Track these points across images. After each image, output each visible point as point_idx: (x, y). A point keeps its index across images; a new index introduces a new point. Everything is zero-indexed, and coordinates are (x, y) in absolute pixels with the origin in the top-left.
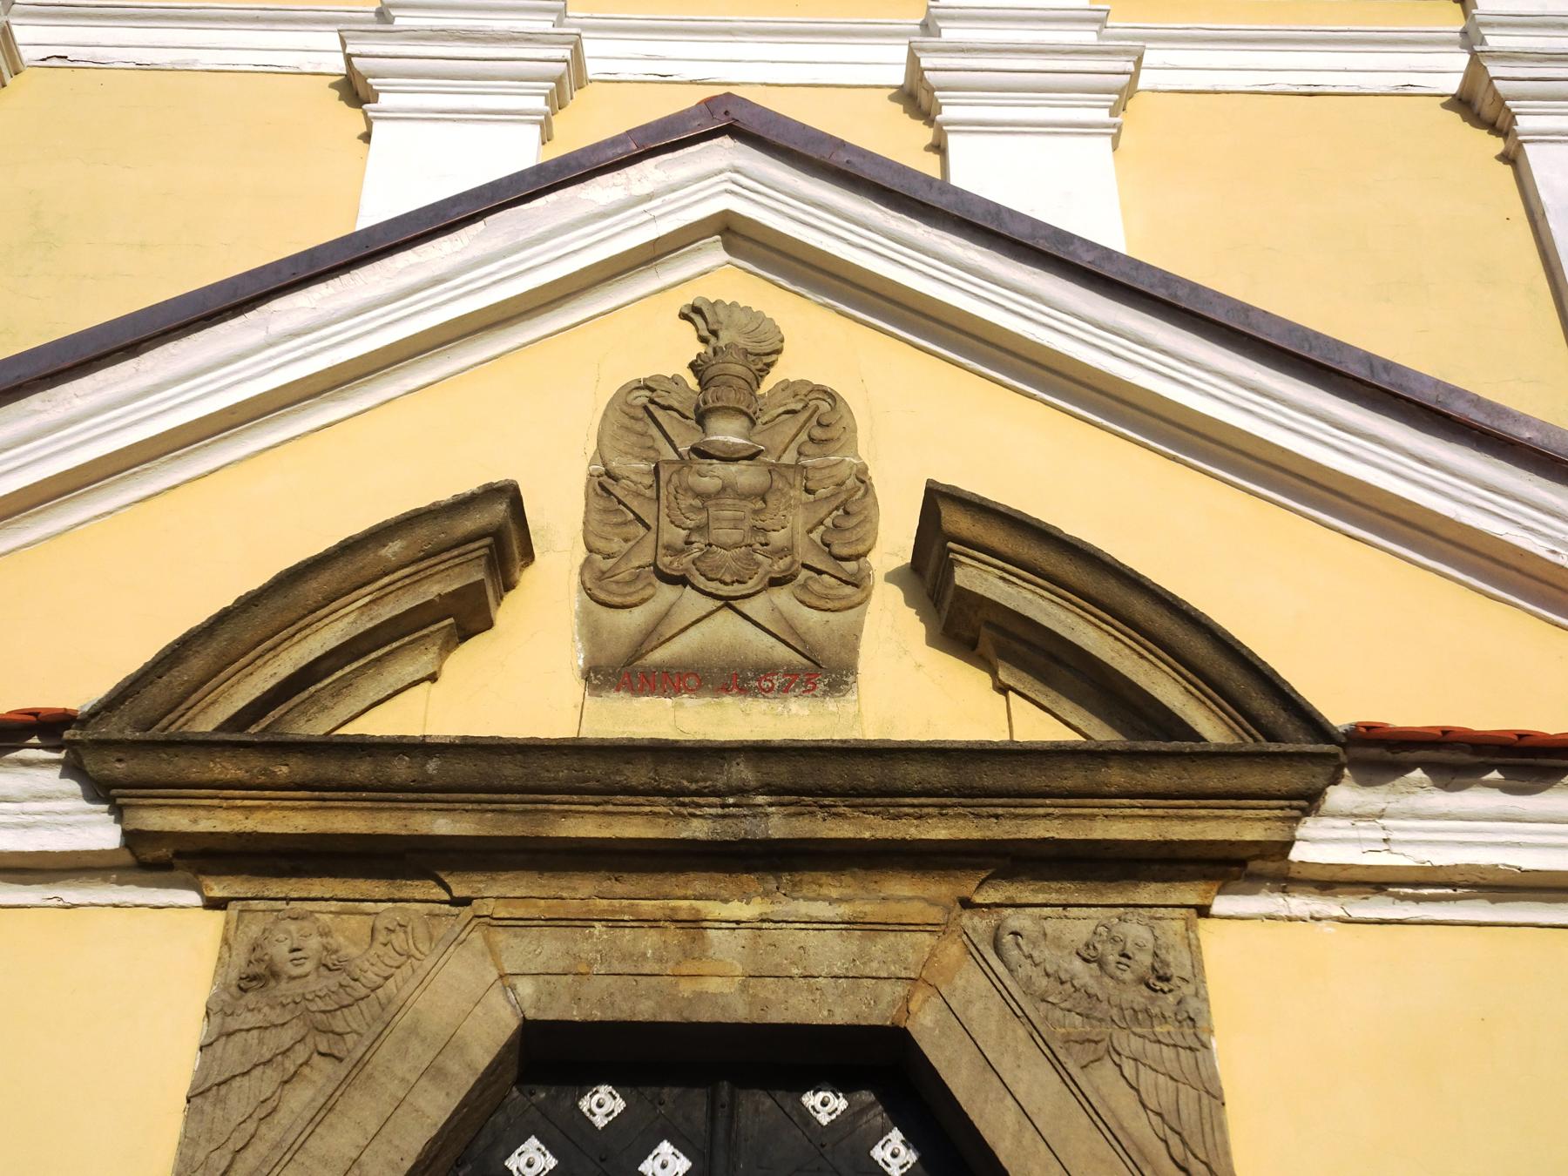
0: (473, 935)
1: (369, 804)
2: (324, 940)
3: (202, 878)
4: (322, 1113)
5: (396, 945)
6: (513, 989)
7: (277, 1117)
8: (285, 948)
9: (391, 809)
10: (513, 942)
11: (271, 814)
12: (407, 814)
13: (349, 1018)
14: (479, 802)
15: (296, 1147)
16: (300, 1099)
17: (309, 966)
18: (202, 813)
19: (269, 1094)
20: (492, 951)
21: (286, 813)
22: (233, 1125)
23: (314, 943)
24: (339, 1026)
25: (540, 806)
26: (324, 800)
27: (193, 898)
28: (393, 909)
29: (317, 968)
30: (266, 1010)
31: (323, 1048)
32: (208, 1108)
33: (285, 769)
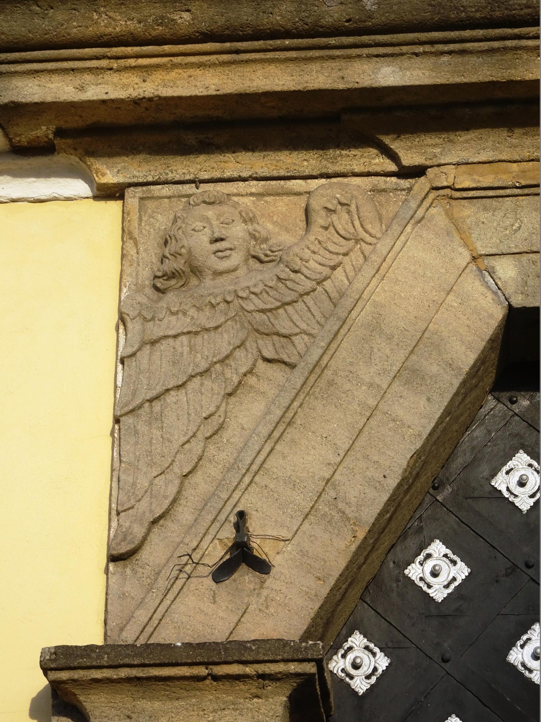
0: (433, 211)
1: (293, 54)
2: (250, 228)
3: (91, 161)
4: (281, 428)
5: (339, 227)
6: (491, 273)
7: (225, 435)
8: (204, 238)
9: (321, 58)
10: (483, 216)
11: (173, 74)
12: (343, 63)
13: (295, 317)
14: (432, 42)
15: (255, 467)
16: (249, 414)
17: (236, 259)
18: (88, 78)
19: (212, 409)
20: (458, 228)
21: (191, 72)
22: (176, 446)
23: (238, 231)
24: (284, 326)
25: (509, 43)
26: (237, 52)
27: (79, 187)
28: (330, 184)
29: (246, 260)
30: (192, 312)
31: (269, 353)
32: (142, 427)
33: (186, 16)
